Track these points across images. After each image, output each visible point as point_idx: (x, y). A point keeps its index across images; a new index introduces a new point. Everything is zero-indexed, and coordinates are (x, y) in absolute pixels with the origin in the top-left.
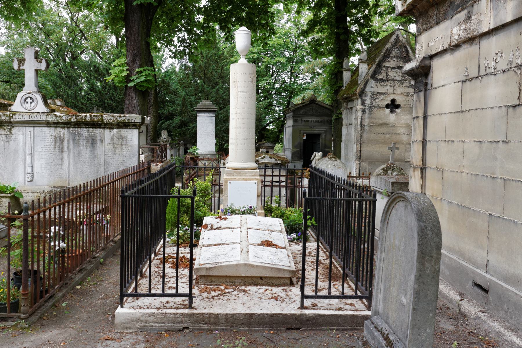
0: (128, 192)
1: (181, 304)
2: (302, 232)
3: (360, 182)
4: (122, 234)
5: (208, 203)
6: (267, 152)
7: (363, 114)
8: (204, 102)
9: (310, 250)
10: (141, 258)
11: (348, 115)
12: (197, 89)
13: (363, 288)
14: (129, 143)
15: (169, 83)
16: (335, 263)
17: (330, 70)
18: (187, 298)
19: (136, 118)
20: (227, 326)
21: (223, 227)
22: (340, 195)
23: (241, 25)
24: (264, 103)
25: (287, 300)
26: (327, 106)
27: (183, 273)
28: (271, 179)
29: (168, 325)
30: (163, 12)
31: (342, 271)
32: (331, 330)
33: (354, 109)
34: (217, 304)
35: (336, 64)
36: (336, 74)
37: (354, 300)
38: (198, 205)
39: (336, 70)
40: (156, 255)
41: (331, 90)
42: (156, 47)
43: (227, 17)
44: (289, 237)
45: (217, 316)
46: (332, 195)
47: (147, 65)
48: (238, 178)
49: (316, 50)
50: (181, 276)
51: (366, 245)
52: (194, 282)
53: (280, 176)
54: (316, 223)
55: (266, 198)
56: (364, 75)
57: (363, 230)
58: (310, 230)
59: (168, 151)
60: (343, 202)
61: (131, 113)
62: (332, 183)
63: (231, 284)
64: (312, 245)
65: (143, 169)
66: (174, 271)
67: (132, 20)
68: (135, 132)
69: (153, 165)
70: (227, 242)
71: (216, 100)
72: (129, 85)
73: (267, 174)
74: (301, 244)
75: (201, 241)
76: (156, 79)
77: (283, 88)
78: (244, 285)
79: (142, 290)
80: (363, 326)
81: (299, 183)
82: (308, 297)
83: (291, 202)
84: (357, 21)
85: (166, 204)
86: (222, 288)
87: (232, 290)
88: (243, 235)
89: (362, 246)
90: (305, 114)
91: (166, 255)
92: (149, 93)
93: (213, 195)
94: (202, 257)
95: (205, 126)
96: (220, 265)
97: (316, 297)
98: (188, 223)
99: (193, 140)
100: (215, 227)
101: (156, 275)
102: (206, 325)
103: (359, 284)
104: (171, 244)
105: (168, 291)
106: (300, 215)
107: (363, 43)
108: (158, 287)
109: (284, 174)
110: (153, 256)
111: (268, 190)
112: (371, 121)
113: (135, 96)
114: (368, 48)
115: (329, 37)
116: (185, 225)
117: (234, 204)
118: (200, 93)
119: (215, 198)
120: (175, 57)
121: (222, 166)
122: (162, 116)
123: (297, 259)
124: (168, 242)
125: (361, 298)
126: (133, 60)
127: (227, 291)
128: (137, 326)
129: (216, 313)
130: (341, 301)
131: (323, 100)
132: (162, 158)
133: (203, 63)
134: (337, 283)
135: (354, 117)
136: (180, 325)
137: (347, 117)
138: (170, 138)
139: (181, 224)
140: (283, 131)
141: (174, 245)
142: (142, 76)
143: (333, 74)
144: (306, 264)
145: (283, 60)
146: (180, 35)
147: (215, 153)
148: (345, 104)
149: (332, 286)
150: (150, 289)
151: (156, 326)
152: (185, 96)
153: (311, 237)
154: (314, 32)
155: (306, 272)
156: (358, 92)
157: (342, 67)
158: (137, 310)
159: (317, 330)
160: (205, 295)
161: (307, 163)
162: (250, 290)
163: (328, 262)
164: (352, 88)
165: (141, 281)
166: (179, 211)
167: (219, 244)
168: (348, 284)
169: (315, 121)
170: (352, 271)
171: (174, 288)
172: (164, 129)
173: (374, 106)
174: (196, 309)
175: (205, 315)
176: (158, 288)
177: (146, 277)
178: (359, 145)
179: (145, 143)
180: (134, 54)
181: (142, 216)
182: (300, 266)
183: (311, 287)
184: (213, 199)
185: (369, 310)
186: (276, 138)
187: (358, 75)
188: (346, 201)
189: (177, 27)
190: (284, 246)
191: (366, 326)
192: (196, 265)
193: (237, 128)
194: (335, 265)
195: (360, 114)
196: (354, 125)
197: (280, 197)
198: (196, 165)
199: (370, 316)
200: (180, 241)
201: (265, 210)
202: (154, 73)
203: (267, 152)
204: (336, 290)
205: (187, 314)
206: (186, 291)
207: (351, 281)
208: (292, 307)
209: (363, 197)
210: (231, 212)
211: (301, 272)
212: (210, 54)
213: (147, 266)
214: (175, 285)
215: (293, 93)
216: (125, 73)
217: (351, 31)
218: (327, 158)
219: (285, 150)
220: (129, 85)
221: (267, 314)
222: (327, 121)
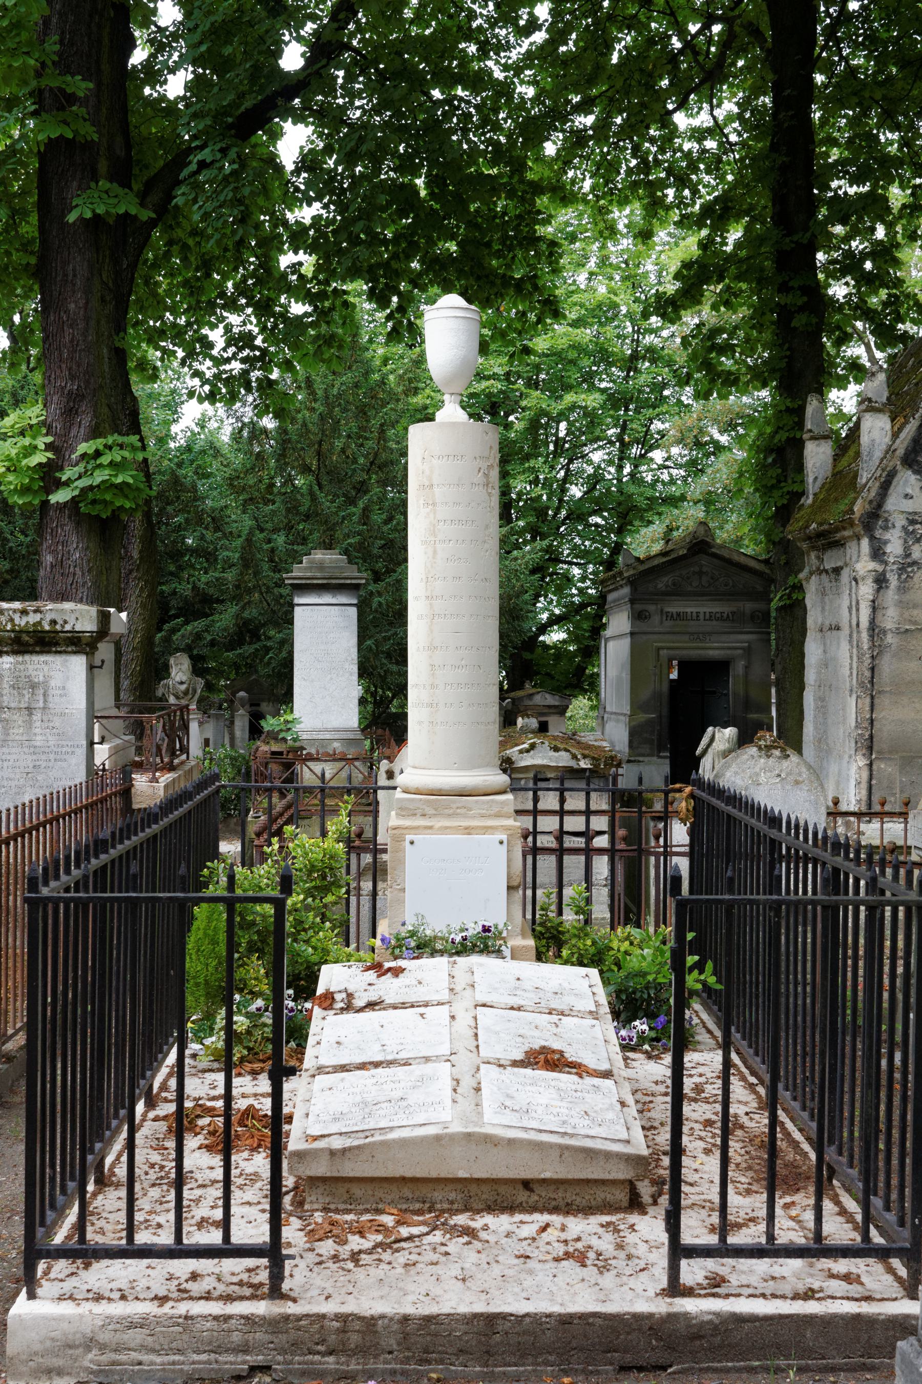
0: (53, 884)
1: (241, 1284)
2: (668, 1014)
3: (871, 833)
4: (30, 1028)
5: (337, 913)
6: (543, 728)
7: (878, 590)
8: (319, 555)
9: (697, 1080)
10: (101, 1116)
11: (824, 594)
12: (292, 508)
13: (892, 1217)
14: (55, 702)
15: (194, 489)
16: (789, 1125)
17: (761, 434)
18: (264, 1261)
19: (80, 616)
20: (407, 1360)
21: (388, 1001)
22: (802, 884)
23: (447, 289)
24: (530, 552)
25: (620, 1263)
26: (753, 564)
27: (249, 1168)
28: (557, 827)
29: (196, 1357)
30: (170, 243)
31: (813, 1156)
32: (778, 1370)
33: (845, 575)
34: (371, 1280)
35: (779, 414)
36: (779, 453)
37: (858, 1260)
38: (299, 922)
39: (783, 436)
40: (151, 1104)
41: (764, 504)
42: (143, 365)
43: (394, 256)
44: (623, 1033)
45: (370, 1323)
46: (774, 884)
47: (117, 430)
48: (439, 823)
49: (708, 366)
50: (240, 1181)
51: (898, 1056)
52: (287, 1200)
53: (588, 813)
54: (719, 981)
55: (539, 892)
56: (878, 454)
57: (885, 1005)
58: (697, 1006)
59: (194, 727)
60: (814, 910)
61: (63, 597)
62: (773, 841)
63: (418, 1206)
64: (704, 1062)
65: (107, 797)
66: (217, 1161)
67: (66, 275)
68: (78, 664)
69: (140, 781)
70: (403, 1055)
71: (361, 544)
72: (54, 498)
73: (541, 806)
74: (668, 1059)
75: (310, 1052)
76: (148, 476)
77: (597, 501)
78: (466, 1209)
79: (102, 1232)
80: (892, 1356)
81: (657, 838)
82: (694, 1252)
83: (628, 908)
84: (849, 266)
85: (185, 920)
86: (388, 1220)
87: (424, 1229)
88: (460, 1030)
89: (884, 1063)
90: (676, 592)
91: (188, 1104)
92: (125, 527)
93: (353, 885)
94: (314, 1110)
95: (323, 640)
96: (378, 1138)
97: (724, 1251)
98: (265, 987)
99: (278, 687)
100: (359, 1003)
101: (153, 1176)
102: (331, 1359)
103: (877, 1202)
104: (204, 1063)
105: (195, 1237)
106: (662, 953)
107: (872, 339)
108: (161, 1219)
109: (605, 807)
110: (140, 1107)
111: (547, 864)
112: (906, 615)
113: (74, 538)
114: (891, 359)
115: (756, 321)
116: (255, 995)
117: (428, 919)
118: (306, 523)
119: (359, 896)
120: (212, 397)
121: (382, 781)
122: (173, 603)
123: (652, 1114)
124: (194, 1056)
125: (882, 1254)
126: (69, 413)
127: (404, 1231)
128: (86, 1364)
129: (367, 1314)
130: (811, 1265)
131: (738, 540)
132: (173, 755)
133: (315, 416)
134: (797, 1198)
135: (845, 603)
136: (240, 1358)
137: (823, 602)
138: (200, 683)
139: (241, 991)
140: (598, 652)
141: (216, 1065)
142: (100, 466)
143: (768, 450)
144: (685, 1129)
145: (593, 400)
146: (234, 319)
147: (359, 736)
148: (813, 555)
149: (778, 1211)
150: (131, 1229)
151: (152, 1363)
152: (251, 533)
153: (700, 1030)
154: (699, 303)
155: (685, 1161)
156: (857, 515)
157: (800, 424)
158: (86, 1307)
159: (728, 1370)
160: (327, 1247)
161: (684, 765)
162: (486, 1228)
163: (760, 1123)
164: (836, 500)
165: (99, 1201)
166: (232, 946)
167: (377, 1065)
168: (838, 1203)
169: (711, 617)
170: (851, 1157)
171: (216, 1224)
172: (178, 650)
173: (914, 563)
174: (295, 1300)
175: (327, 1323)
176: (159, 1226)
177: (118, 1185)
178: (868, 700)
179: (112, 702)
180: (70, 393)
181: (102, 964)
182: (664, 1137)
183: (704, 1213)
184: (353, 900)
185: (913, 1297)
186: (574, 675)
187: (858, 454)
188: (824, 908)
189: (222, 295)
190: (605, 1066)
191: (903, 1360)
192: (294, 1143)
193: (432, 648)
194: (788, 1135)
195: (866, 590)
196: (846, 631)
197: (588, 889)
198: (290, 780)
199: (916, 1318)
200: (238, 1052)
201: (538, 936)
202: (140, 456)
203: (543, 728)
204: (792, 1224)
205: (263, 1318)
206: (260, 1234)
207: (848, 1190)
208: (639, 1288)
209: (882, 893)
210: (418, 947)
211: (666, 1161)
212: (337, 384)
213: (119, 1144)
214: (218, 1214)
215: (628, 512)
216: (40, 458)
217: (832, 300)
218: (753, 750)
219: (604, 718)
220: (54, 498)
221: (549, 1316)
222: (753, 617)
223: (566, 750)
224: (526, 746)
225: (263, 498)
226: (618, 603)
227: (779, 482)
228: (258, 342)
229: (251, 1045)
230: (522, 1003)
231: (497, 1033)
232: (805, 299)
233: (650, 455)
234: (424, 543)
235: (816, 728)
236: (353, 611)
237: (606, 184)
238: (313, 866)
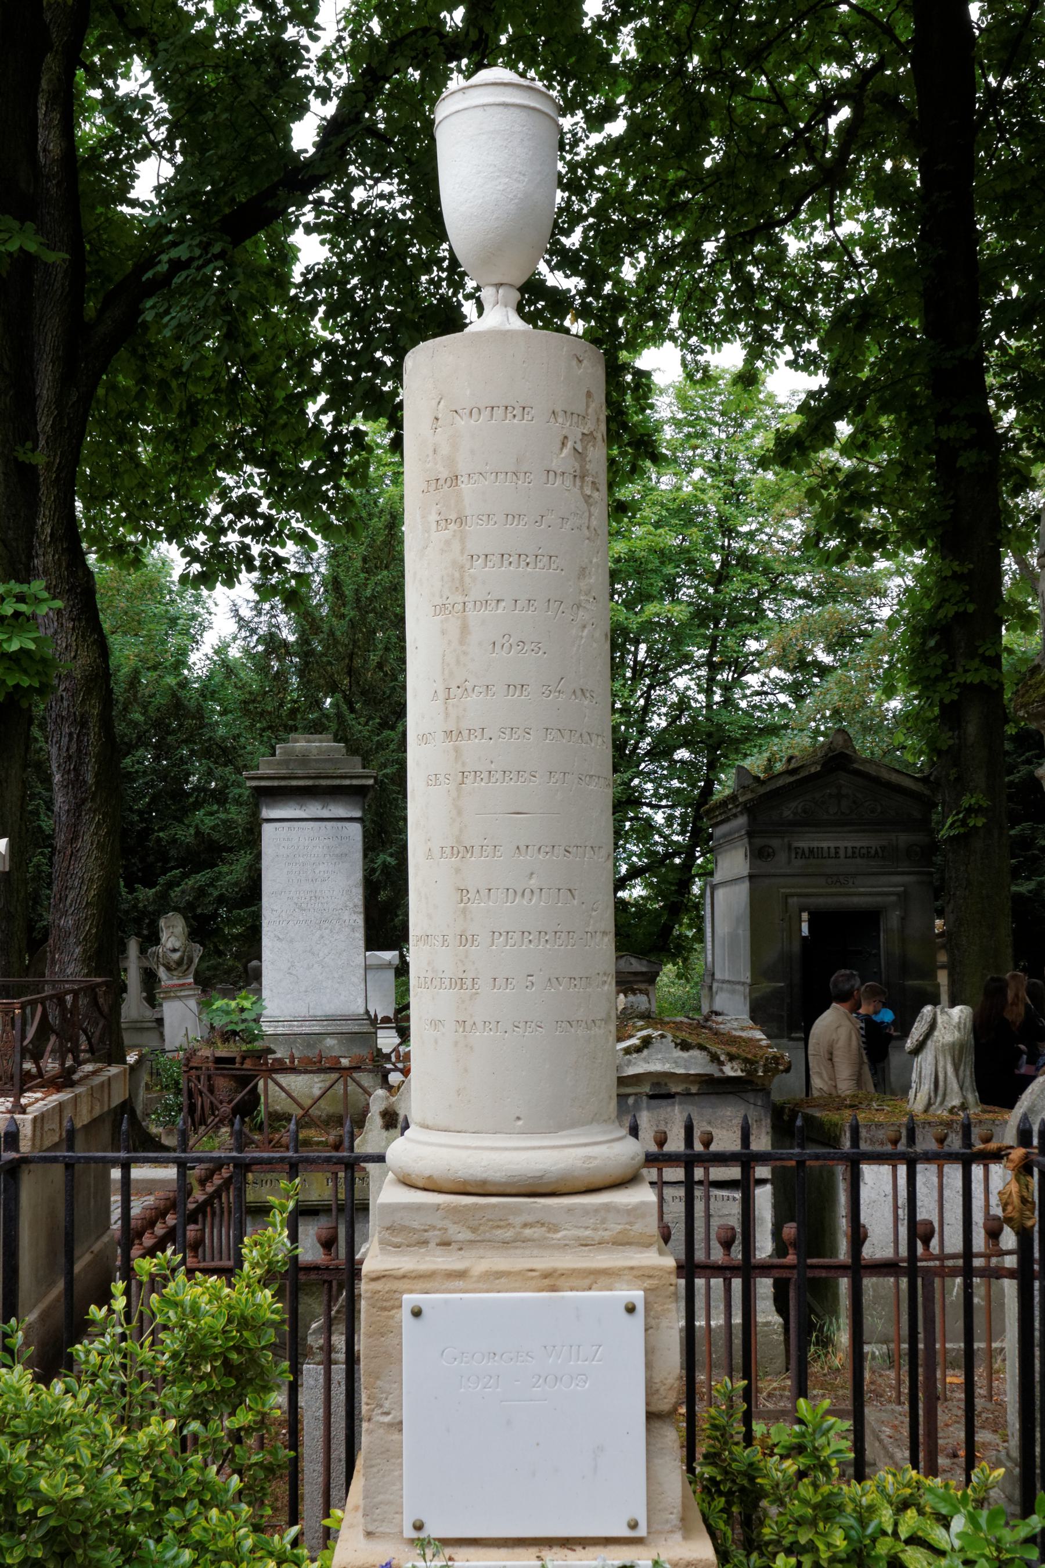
48: (483, 1262)
90: (808, 822)
122: (173, 852)
138: (198, 950)
169: (855, 853)
193: (461, 850)
223: (702, 1048)
224: (634, 1041)
225: (285, 726)
226: (729, 840)
227: (946, 671)
228: (264, 507)
232: (974, 431)
233: (744, 678)
234: (441, 609)
236: (355, 831)
237: (699, 319)
238: (204, 1347)
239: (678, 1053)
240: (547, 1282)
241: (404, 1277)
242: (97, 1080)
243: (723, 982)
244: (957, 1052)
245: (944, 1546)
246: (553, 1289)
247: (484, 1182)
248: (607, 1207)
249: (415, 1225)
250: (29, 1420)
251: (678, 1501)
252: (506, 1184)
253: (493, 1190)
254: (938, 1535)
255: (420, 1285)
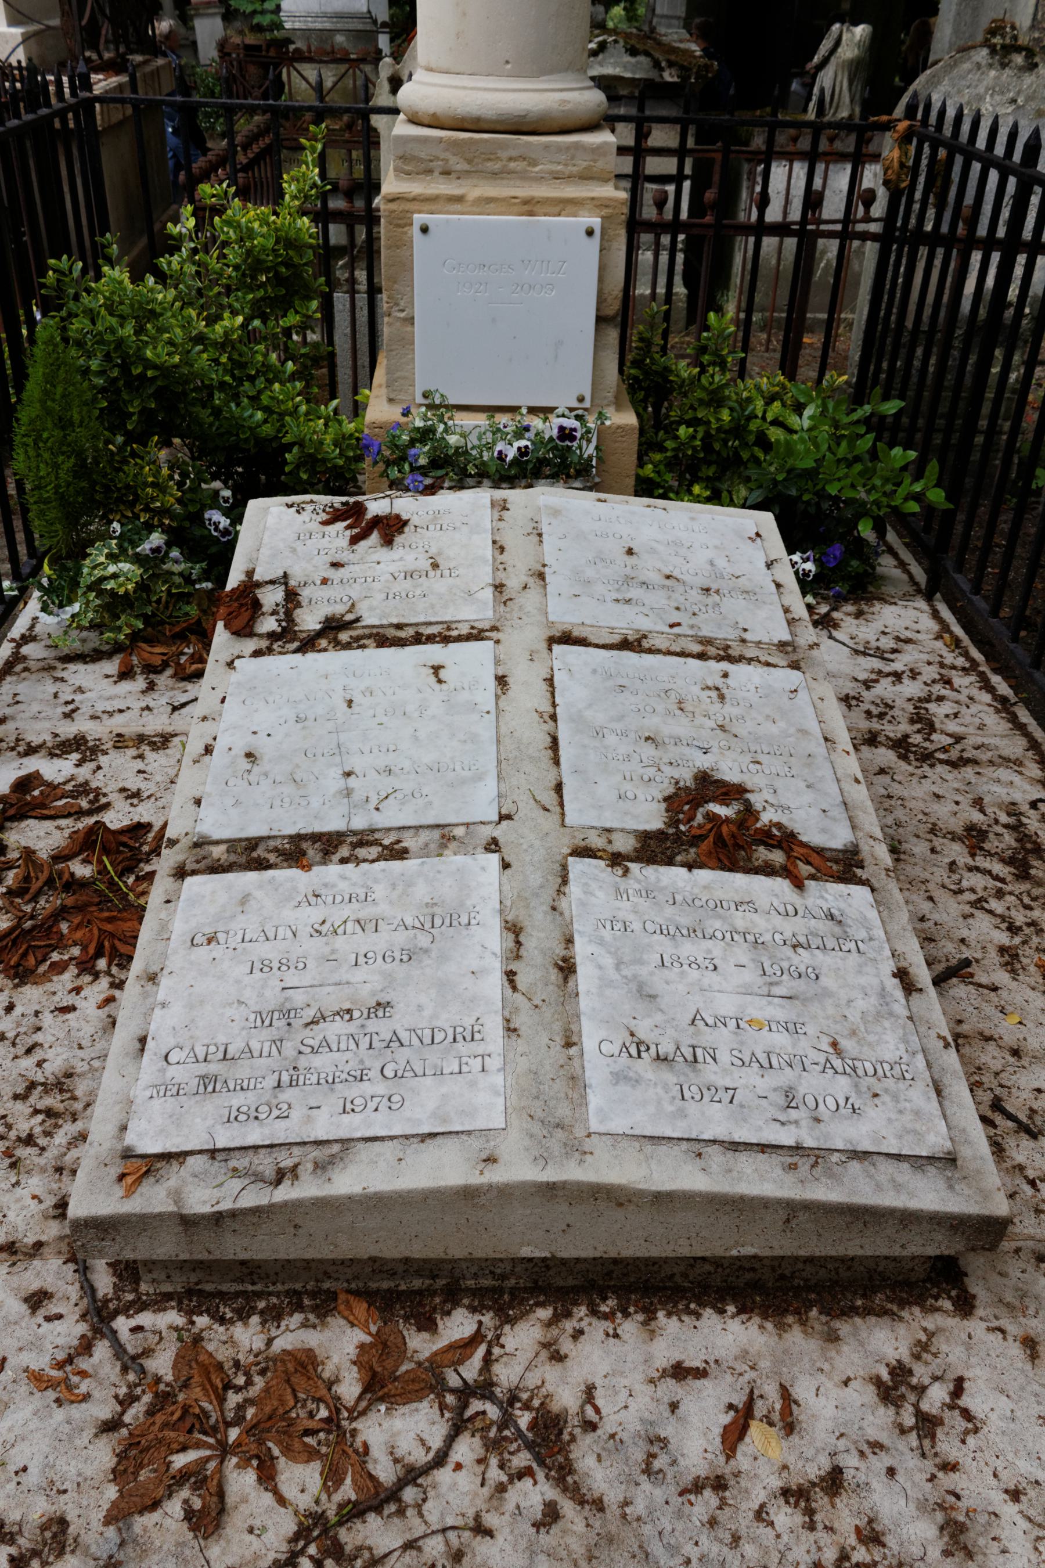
48: (475, 190)
100: (309, 620)
121: (382, 97)
223: (647, 54)
229: (149, 610)
230: (645, 624)
231: (599, 733)
235: (956, 31)
238: (259, 261)
239: (627, 58)
240: (526, 208)
241: (414, 199)
242: (148, 69)
243: (662, 16)
244: (855, 68)
245: (796, 427)
246: (531, 214)
247: (478, 120)
248: (577, 146)
249: (423, 155)
250: (132, 306)
251: (614, 390)
252: (497, 121)
253: (486, 127)
254: (793, 420)
255: (427, 207)
